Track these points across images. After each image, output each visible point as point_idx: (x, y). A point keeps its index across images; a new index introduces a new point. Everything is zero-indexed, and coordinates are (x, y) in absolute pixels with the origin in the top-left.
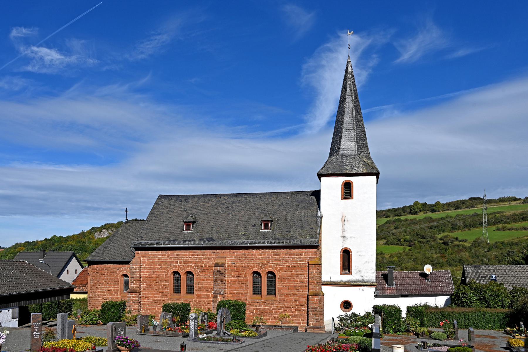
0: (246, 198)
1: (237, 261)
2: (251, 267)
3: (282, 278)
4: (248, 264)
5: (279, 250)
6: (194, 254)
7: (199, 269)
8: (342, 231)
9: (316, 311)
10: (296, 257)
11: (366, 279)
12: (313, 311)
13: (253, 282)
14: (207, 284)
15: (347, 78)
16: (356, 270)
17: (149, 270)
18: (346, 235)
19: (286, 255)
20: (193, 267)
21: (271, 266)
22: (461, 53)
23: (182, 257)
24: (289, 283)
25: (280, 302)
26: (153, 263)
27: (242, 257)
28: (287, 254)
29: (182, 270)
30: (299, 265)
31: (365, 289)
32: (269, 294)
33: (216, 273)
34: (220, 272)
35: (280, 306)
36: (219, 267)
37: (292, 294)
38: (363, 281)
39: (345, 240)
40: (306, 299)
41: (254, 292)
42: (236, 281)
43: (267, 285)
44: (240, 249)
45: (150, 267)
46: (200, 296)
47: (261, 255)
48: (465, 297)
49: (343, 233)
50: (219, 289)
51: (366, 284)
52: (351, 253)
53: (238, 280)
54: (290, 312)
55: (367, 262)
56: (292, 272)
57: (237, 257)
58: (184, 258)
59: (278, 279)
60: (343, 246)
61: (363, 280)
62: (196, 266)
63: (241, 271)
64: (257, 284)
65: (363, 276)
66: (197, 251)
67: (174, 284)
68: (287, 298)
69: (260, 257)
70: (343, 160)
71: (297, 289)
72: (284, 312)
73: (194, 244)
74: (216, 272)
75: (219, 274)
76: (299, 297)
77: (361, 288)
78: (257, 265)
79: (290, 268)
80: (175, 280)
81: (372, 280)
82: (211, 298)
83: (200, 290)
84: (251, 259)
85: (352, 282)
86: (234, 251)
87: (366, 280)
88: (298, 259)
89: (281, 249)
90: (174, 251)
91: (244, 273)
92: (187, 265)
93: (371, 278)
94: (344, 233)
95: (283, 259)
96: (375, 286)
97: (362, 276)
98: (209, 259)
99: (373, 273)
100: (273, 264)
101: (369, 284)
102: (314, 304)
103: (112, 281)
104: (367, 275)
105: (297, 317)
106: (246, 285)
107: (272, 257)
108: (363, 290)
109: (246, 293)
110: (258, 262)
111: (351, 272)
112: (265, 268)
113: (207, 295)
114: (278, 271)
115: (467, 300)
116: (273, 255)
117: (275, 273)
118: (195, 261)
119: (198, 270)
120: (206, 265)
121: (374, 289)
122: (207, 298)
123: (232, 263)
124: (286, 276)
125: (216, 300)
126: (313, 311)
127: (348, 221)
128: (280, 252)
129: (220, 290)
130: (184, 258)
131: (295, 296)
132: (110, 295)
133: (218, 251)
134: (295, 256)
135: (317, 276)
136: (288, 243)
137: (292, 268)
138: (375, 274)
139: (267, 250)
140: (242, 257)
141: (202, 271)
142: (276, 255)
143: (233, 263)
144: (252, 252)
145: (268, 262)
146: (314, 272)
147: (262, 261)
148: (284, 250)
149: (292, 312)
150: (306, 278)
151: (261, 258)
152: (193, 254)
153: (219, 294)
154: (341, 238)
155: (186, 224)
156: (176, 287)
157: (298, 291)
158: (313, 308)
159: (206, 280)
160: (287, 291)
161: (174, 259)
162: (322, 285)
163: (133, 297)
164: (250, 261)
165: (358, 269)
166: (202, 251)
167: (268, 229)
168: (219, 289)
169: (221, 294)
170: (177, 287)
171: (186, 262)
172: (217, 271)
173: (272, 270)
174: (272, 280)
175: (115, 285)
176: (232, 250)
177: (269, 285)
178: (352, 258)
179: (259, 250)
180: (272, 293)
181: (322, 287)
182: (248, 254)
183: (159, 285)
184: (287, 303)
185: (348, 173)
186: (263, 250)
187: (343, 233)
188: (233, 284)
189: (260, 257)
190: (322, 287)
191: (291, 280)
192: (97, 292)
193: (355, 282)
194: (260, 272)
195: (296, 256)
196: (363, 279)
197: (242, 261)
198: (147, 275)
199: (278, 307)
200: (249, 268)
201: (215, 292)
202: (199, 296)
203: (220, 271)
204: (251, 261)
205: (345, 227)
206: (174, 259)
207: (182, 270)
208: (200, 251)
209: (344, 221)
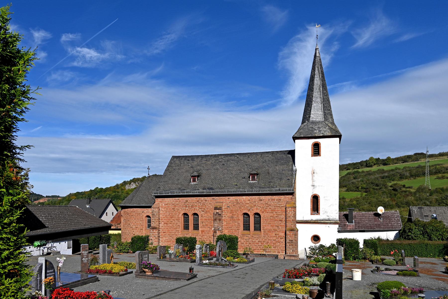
1: (231, 205)
2: (242, 209)
3: (265, 218)
4: (240, 207)
5: (263, 197)
9: (292, 243)
10: (277, 202)
11: (331, 218)
14: (209, 223)
16: (323, 211)
17: (166, 212)
18: (315, 184)
19: (269, 200)
20: (198, 210)
21: (191, 211)
22: (406, 37)
23: (190, 203)
24: (271, 222)
26: (168, 207)
27: (235, 202)
29: (190, 212)
37: (274, 230)
40: (284, 234)
42: (231, 220)
43: (254, 223)
45: (166, 210)
47: (249, 200)
51: (331, 222)
56: (273, 213)
58: (192, 203)
60: (313, 193)
61: (328, 219)
64: (246, 223)
65: (329, 216)
67: (184, 222)
69: (248, 202)
74: (215, 214)
76: (279, 232)
77: (328, 225)
83: (204, 227)
85: (320, 220)
86: (229, 197)
93: (335, 217)
95: (267, 204)
98: (210, 204)
101: (333, 222)
102: (291, 238)
103: (139, 221)
105: (278, 248)
106: (238, 223)
107: (258, 202)
108: (329, 227)
109: (238, 229)
110: (247, 205)
112: (253, 210)
114: (263, 212)
123: (227, 207)
127: (317, 173)
128: (264, 198)
129: (219, 227)
130: (192, 203)
132: (137, 231)
133: (217, 197)
138: (338, 214)
139: (254, 197)
140: (235, 202)
142: (261, 200)
143: (228, 207)
145: (255, 205)
151: (250, 202)
157: (278, 228)
158: (289, 241)
160: (269, 227)
161: (184, 204)
163: (154, 232)
167: (255, 180)
172: (216, 213)
173: (258, 212)
174: (247, 219)
175: (141, 224)
177: (256, 223)
178: (320, 202)
181: (297, 224)
183: (173, 223)
189: (248, 202)
190: (297, 224)
191: (272, 220)
192: (128, 229)
193: (322, 220)
194: (249, 213)
197: (235, 205)
198: (164, 216)
202: (202, 231)
203: (218, 213)
204: (242, 205)
205: (314, 178)
207: (190, 212)
209: (314, 173)
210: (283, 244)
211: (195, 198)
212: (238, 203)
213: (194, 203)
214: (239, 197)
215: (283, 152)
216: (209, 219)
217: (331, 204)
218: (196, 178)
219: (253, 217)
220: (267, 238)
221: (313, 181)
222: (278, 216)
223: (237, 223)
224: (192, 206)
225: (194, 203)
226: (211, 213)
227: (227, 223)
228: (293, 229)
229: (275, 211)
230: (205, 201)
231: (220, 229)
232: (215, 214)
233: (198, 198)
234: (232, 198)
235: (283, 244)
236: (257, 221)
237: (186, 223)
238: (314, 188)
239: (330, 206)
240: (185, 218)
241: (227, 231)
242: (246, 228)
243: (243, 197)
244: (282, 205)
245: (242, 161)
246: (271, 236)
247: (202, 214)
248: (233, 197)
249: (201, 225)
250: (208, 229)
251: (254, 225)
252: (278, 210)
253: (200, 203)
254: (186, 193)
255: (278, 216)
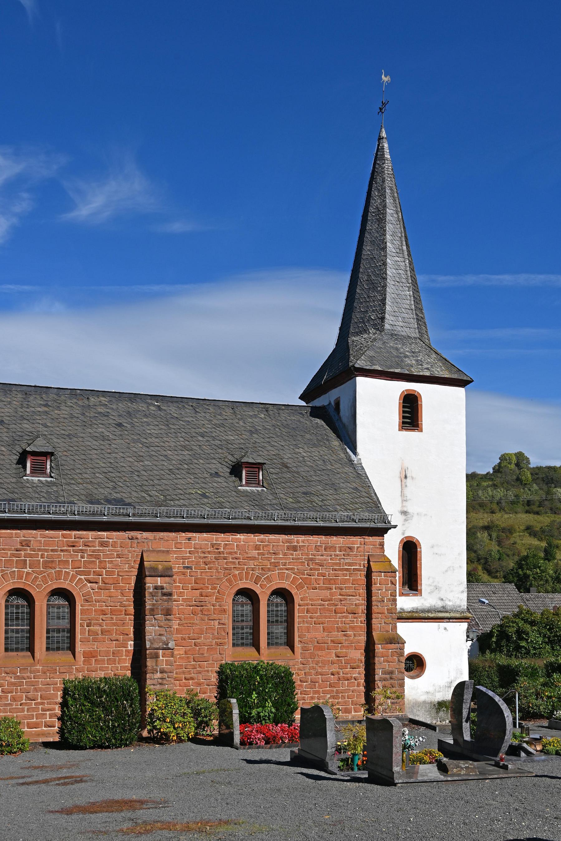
0: (159, 406)
1: (197, 563)
2: (235, 576)
3: (307, 604)
4: (226, 569)
5: (302, 538)
6: (76, 542)
7: (90, 582)
8: (401, 501)
9: (391, 678)
10: (340, 555)
11: (449, 604)
12: (385, 680)
13: (234, 617)
14: (114, 624)
15: (383, 172)
16: (430, 585)
18: (410, 508)
19: (317, 548)
20: (74, 577)
21: (45, 581)
22: (177, 227)
23: (39, 550)
24: (326, 617)
25: (305, 662)
28: (319, 546)
29: (39, 586)
30: (346, 574)
31: (450, 626)
32: (272, 644)
33: (151, 593)
34: (163, 589)
35: (303, 672)
36: (161, 576)
37: (332, 641)
38: (444, 610)
39: (407, 520)
40: (361, 654)
41: (235, 642)
42: (194, 613)
43: (268, 621)
44: (206, 532)
46: (94, 657)
47: (257, 548)
48: (522, 639)
49: (402, 503)
50: (160, 635)
51: (452, 615)
52: (421, 548)
53: (201, 611)
54: (327, 684)
55: (451, 568)
56: (331, 589)
57: (198, 552)
58: (47, 551)
59: (299, 606)
60: (403, 534)
61: (443, 607)
62: (81, 573)
63: (207, 587)
64: (242, 621)
65: (444, 599)
66: (85, 533)
68: (320, 653)
69: (255, 553)
70: (397, 344)
71: (344, 630)
72: (313, 687)
73: (79, 514)
74: (151, 590)
75: (160, 594)
76: (347, 647)
77: (443, 625)
78: (247, 573)
79: (326, 579)
80: (12, 613)
81: (460, 606)
82: (126, 659)
83: (94, 640)
84: (233, 558)
85: (423, 611)
86: (190, 535)
87: (449, 608)
88: (344, 559)
89: (305, 535)
90: (14, 532)
91: (214, 593)
92: (53, 571)
93: (458, 603)
94: (405, 504)
95: (312, 560)
96: (468, 619)
97: (442, 599)
98: (119, 556)
99: (463, 592)
100: (287, 569)
101: (458, 615)
104: (450, 596)
105: (343, 697)
107: (285, 554)
108: (445, 629)
110: (252, 564)
111: (421, 590)
112: (269, 579)
113: (113, 653)
114: (300, 587)
115: (528, 643)
116: (288, 548)
117: (293, 593)
118: (81, 561)
119: (89, 585)
120: (112, 573)
121: (465, 626)
122: (115, 660)
123: (184, 567)
124: (318, 599)
125: (154, 664)
126: (385, 680)
127: (412, 478)
128: (303, 542)
129: (164, 638)
130: (47, 551)
131: (338, 646)
133: (145, 534)
134: (338, 552)
135: (389, 599)
136: (323, 519)
137: (331, 579)
138: (465, 595)
139: (272, 537)
141: (100, 588)
142: (295, 549)
143: (188, 568)
144: (237, 539)
145: (276, 565)
146: (384, 590)
147: (260, 562)
148: (311, 538)
149: (331, 686)
150: (362, 605)
151: (258, 554)
152: (73, 542)
153: (164, 649)
154: (399, 515)
155: (32, 457)
156: (241, 631)
157: (345, 635)
158: (384, 673)
159: (112, 612)
160: (319, 634)
161: (13, 555)
162: (398, 619)
164: (231, 562)
165: (434, 584)
166: (99, 533)
168: (160, 635)
169: (169, 649)
170: (58, 635)
171: (52, 561)
172: (156, 588)
173: (285, 584)
174: (245, 608)
176: (184, 534)
177: (272, 622)
178: (421, 560)
179: (252, 536)
180: (279, 641)
181: (399, 625)
182: (226, 544)
184: (320, 665)
185: (415, 374)
186: (262, 536)
187: (404, 505)
188: (186, 622)
189: (255, 553)
190: (399, 625)
191: (329, 610)
193: (429, 611)
194: (257, 589)
195: (341, 551)
196: (444, 605)
197: (210, 562)
199: (299, 675)
200: (229, 581)
201: (152, 643)
202: (89, 656)
203: (162, 588)
205: (407, 492)
206: (13, 555)
207: (39, 586)
208: (93, 533)
209: (406, 477)
210: (358, 685)
211: (60, 533)
212: (219, 556)
213: (56, 551)
214: (222, 535)
215: (294, 408)
216: (115, 611)
217: (449, 567)
218: (48, 463)
219: (45, 602)
220: (314, 668)
221: (403, 501)
222: (346, 599)
223: (216, 622)
224: (47, 565)
225: (56, 551)
226: (122, 590)
227: (184, 622)
228: (394, 639)
229: (335, 582)
230: (102, 544)
231: (170, 645)
232: (151, 590)
233: (74, 533)
234: (199, 538)
235: (358, 685)
236: (277, 616)
237: (17, 625)
238: (406, 520)
239: (447, 571)
240: (12, 606)
241: (181, 652)
242: (242, 639)
243: (238, 536)
244: (355, 564)
245: (181, 422)
246: (324, 662)
247: (88, 593)
248: (205, 535)
249: (82, 633)
250: (113, 646)
251: (268, 628)
252: (345, 581)
253: (82, 551)
254: (29, 513)
255: (346, 599)
